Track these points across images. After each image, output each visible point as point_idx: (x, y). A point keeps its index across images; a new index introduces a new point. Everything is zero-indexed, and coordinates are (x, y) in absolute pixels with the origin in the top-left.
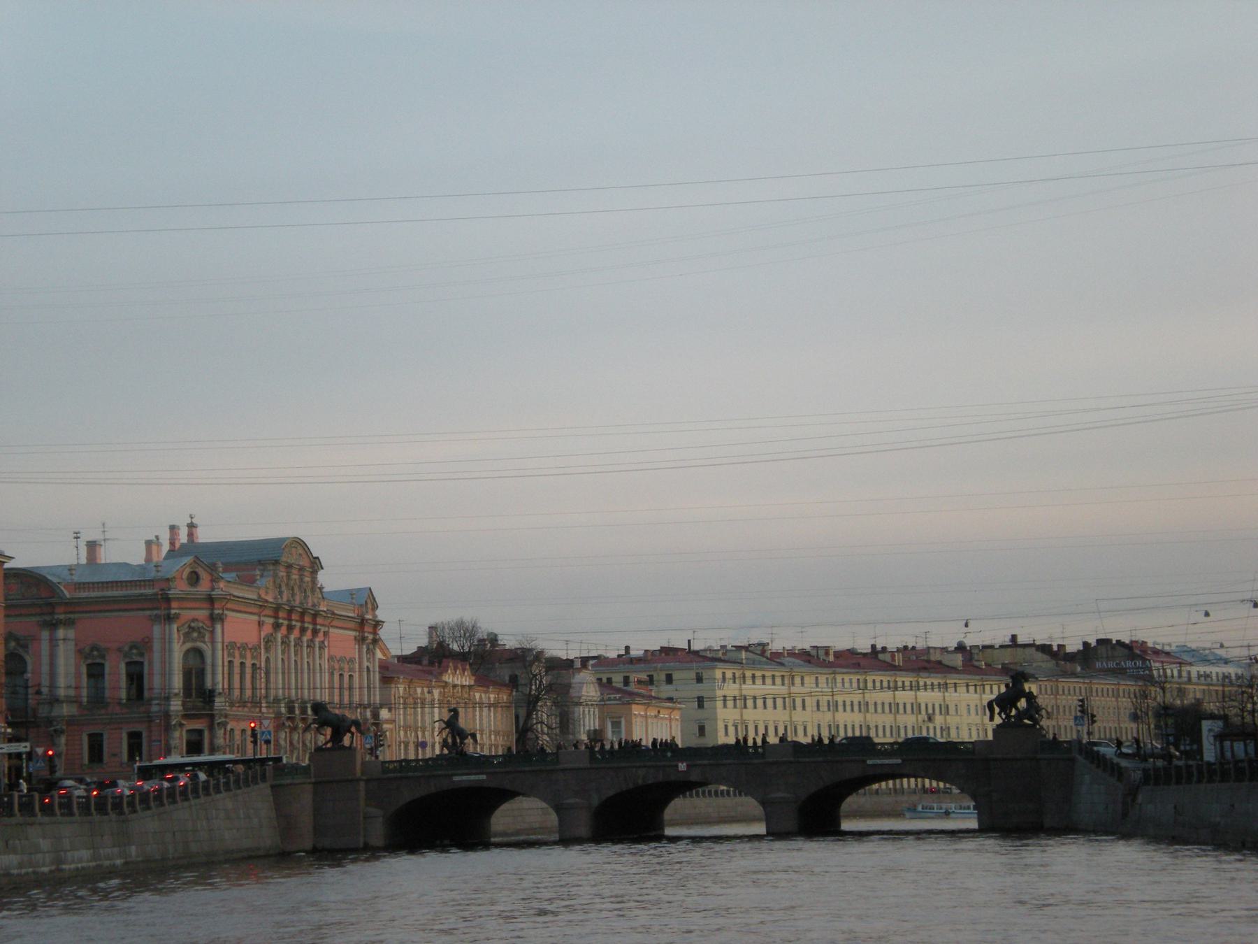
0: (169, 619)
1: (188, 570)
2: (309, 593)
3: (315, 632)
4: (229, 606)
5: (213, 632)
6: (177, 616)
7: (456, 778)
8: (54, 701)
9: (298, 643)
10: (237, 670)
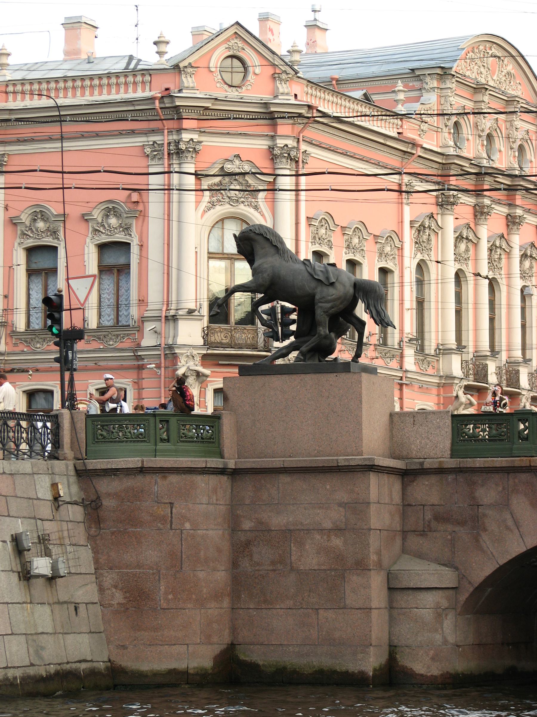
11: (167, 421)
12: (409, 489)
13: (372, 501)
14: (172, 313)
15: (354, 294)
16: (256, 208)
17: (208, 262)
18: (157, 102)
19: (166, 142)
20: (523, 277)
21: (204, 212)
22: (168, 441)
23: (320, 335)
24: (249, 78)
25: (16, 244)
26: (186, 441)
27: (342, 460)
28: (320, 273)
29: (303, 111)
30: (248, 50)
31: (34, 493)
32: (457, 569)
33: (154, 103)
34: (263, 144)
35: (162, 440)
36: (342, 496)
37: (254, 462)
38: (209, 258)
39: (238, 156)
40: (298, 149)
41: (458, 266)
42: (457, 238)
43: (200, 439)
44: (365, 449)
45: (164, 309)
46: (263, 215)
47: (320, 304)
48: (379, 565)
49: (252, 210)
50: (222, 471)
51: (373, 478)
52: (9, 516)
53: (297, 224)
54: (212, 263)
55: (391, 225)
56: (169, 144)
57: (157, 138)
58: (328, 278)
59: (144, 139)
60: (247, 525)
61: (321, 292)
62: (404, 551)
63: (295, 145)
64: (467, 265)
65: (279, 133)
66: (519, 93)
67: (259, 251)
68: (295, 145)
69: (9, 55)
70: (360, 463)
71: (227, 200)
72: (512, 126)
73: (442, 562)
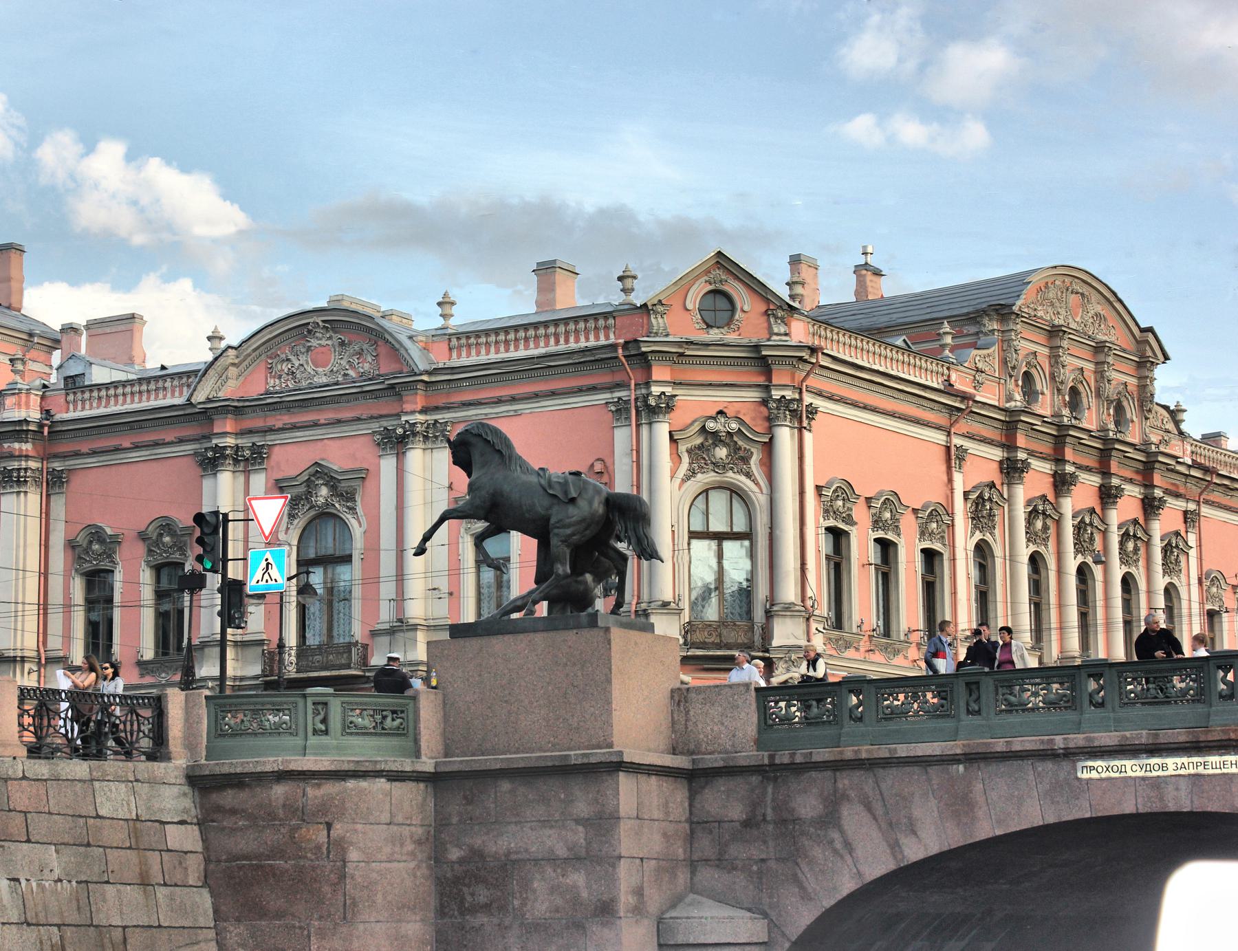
0: (651, 411)
1: (699, 289)
2: (1131, 412)
3: (1150, 506)
4: (813, 381)
5: (769, 447)
6: (668, 405)
7: (1094, 770)
8: (401, 627)
9: (1134, 535)
10: (862, 548)
11: (326, 704)
12: (698, 797)
13: (622, 814)
14: (644, 606)
15: (608, 518)
16: (749, 475)
17: (689, 544)
18: (620, 351)
19: (633, 397)
20: (1123, 561)
21: (683, 481)
22: (326, 732)
23: (558, 575)
24: (737, 317)
25: (462, 530)
26: (357, 734)
27: (575, 756)
28: (557, 487)
29: (805, 354)
30: (732, 281)
31: (91, 808)
32: (765, 915)
33: (616, 351)
34: (754, 395)
35: (315, 732)
36: (582, 808)
37: (461, 762)
38: (690, 538)
39: (721, 412)
40: (800, 400)
41: (1033, 548)
42: (1030, 512)
43: (379, 730)
44: (615, 740)
45: (634, 602)
46: (757, 484)
47: (556, 531)
48: (638, 910)
49: (743, 478)
50: (417, 777)
51: (625, 782)
52: (28, 841)
53: (802, 493)
54: (694, 542)
55: (935, 495)
56: (636, 399)
57: (622, 394)
58: (566, 493)
59: (608, 396)
60: (454, 854)
61: (556, 515)
62: (693, 889)
63: (797, 396)
64: (1046, 546)
65: (774, 382)
66: (1113, 339)
67: (476, 458)
68: (797, 396)
69: (453, 304)
70: (603, 759)
71: (711, 467)
72: (1103, 377)
73: (746, 905)
